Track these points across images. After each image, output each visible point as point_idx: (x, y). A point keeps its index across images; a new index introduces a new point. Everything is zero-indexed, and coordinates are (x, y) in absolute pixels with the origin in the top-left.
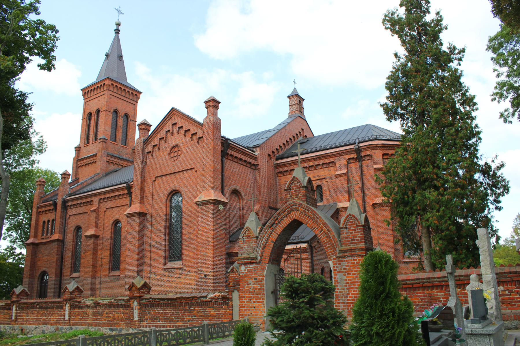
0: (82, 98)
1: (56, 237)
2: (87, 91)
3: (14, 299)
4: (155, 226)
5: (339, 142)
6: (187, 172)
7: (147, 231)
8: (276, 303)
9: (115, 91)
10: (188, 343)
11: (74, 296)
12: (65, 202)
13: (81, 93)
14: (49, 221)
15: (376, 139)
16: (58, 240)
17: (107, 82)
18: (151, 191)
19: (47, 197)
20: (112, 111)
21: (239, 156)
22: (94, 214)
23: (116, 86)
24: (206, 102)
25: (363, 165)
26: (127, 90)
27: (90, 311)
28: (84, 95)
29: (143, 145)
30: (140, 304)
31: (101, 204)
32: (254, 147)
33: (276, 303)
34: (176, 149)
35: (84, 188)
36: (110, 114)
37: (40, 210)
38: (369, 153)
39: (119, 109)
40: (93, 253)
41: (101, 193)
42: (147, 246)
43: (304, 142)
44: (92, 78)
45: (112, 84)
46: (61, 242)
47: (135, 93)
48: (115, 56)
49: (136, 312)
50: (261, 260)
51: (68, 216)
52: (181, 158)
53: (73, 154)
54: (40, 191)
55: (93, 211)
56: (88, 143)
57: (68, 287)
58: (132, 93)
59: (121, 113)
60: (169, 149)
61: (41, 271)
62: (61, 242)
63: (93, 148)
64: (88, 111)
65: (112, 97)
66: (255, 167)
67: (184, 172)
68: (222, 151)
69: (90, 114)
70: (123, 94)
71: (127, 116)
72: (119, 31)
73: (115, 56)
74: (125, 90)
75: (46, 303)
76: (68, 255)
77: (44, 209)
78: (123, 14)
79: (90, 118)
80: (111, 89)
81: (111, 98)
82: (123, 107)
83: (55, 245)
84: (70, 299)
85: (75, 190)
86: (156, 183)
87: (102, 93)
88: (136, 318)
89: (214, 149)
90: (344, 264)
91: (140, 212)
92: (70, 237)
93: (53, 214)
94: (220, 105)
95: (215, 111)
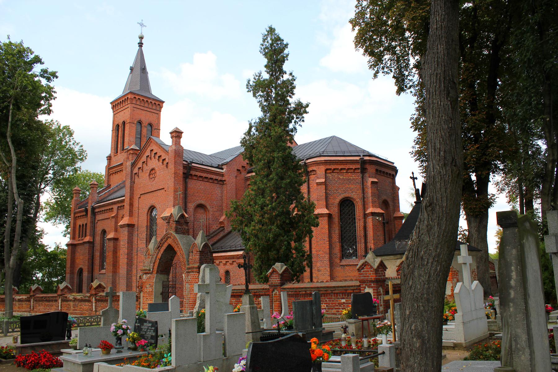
1: (87, 239)
3: (32, 294)
4: (140, 235)
5: (320, 150)
6: (160, 191)
7: (135, 238)
9: (138, 103)
10: (88, 326)
11: (64, 293)
12: (93, 209)
13: (110, 106)
14: (83, 225)
15: (320, 156)
16: (89, 242)
18: (137, 206)
19: (82, 204)
21: (204, 175)
22: (114, 220)
23: (139, 99)
24: (171, 133)
25: (310, 180)
26: (149, 101)
27: (72, 303)
28: (113, 108)
29: (131, 168)
30: (96, 300)
31: (119, 211)
32: (223, 165)
34: (154, 172)
35: (107, 197)
36: (134, 125)
37: (76, 215)
38: (314, 168)
39: (143, 119)
40: (113, 253)
41: (118, 202)
42: (135, 251)
44: (118, 92)
45: (135, 98)
46: (91, 244)
47: (157, 103)
48: (140, 70)
49: (94, 304)
50: (153, 271)
51: (96, 221)
52: (156, 179)
53: (105, 163)
54: (76, 199)
55: (113, 217)
56: (117, 153)
58: (155, 103)
59: (145, 123)
60: (149, 171)
61: (79, 267)
62: (91, 244)
63: (121, 158)
65: (135, 109)
66: (222, 182)
67: (158, 191)
68: (184, 173)
69: (118, 126)
71: (150, 125)
73: (140, 70)
74: (147, 101)
75: (49, 297)
76: (97, 254)
77: (79, 215)
78: (145, 26)
79: (119, 129)
80: (134, 102)
82: (146, 117)
83: (87, 246)
84: (61, 295)
85: (102, 197)
86: (140, 199)
87: (126, 107)
88: (94, 310)
89: (175, 173)
90: (190, 277)
91: (128, 224)
92: (98, 238)
93: (86, 219)
94: (183, 134)
95: (178, 140)
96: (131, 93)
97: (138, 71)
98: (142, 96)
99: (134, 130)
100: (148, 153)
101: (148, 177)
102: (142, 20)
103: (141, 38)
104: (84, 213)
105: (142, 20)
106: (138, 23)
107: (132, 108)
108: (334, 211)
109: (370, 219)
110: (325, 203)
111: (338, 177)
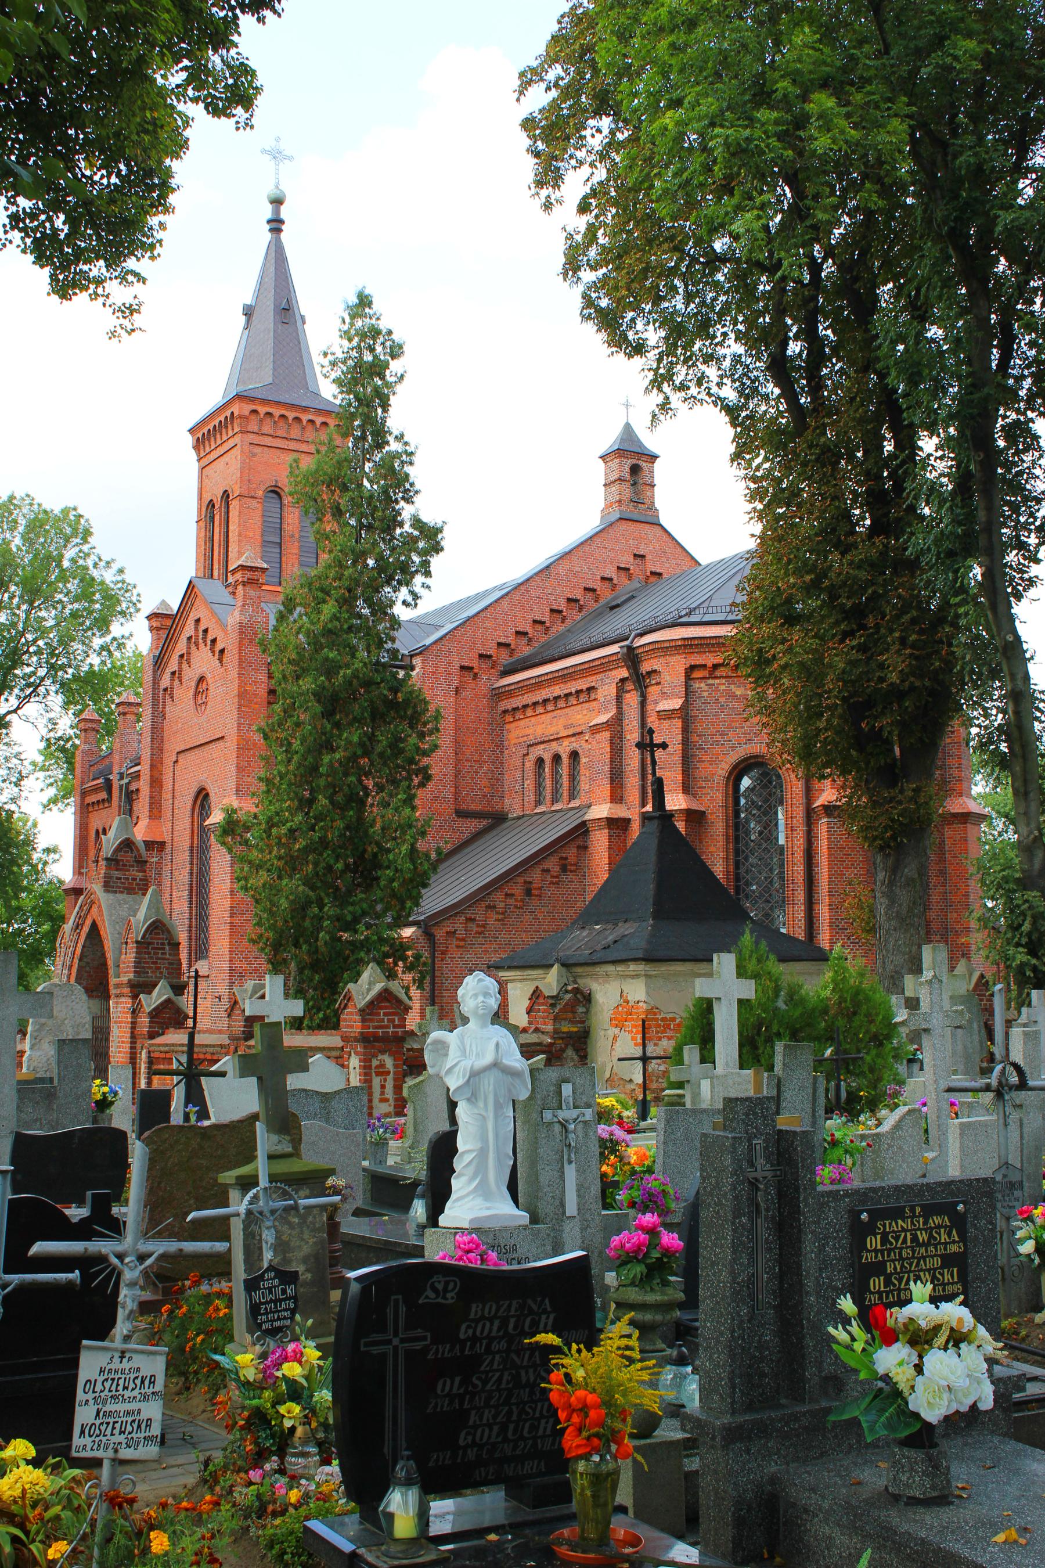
0: (193, 455)
2: (200, 435)
8: (644, 1046)
9: (267, 429)
13: (189, 440)
14: (557, 758)
17: (236, 409)
20: (260, 493)
23: (268, 414)
26: (305, 418)
28: (198, 445)
29: (154, 672)
33: (644, 1046)
36: (254, 504)
43: (617, 606)
44: (209, 393)
57: (353, 993)
64: (207, 498)
65: (258, 450)
69: (211, 504)
70: (296, 433)
72: (282, 222)
74: (297, 419)
79: (214, 513)
80: (253, 426)
81: (254, 455)
96: (239, 397)
97: (267, 318)
98: (278, 403)
99: (256, 521)
100: (189, 630)
101: (192, 702)
102: (278, 140)
103: (277, 202)
104: (103, 795)
105: (278, 140)
106: (264, 151)
107: (246, 448)
108: (711, 800)
109: (823, 825)
110: (680, 777)
111: (728, 691)
